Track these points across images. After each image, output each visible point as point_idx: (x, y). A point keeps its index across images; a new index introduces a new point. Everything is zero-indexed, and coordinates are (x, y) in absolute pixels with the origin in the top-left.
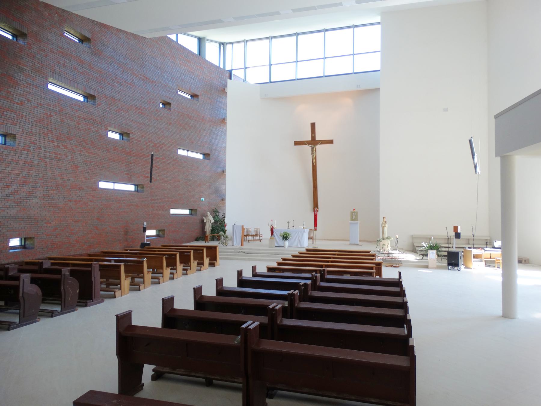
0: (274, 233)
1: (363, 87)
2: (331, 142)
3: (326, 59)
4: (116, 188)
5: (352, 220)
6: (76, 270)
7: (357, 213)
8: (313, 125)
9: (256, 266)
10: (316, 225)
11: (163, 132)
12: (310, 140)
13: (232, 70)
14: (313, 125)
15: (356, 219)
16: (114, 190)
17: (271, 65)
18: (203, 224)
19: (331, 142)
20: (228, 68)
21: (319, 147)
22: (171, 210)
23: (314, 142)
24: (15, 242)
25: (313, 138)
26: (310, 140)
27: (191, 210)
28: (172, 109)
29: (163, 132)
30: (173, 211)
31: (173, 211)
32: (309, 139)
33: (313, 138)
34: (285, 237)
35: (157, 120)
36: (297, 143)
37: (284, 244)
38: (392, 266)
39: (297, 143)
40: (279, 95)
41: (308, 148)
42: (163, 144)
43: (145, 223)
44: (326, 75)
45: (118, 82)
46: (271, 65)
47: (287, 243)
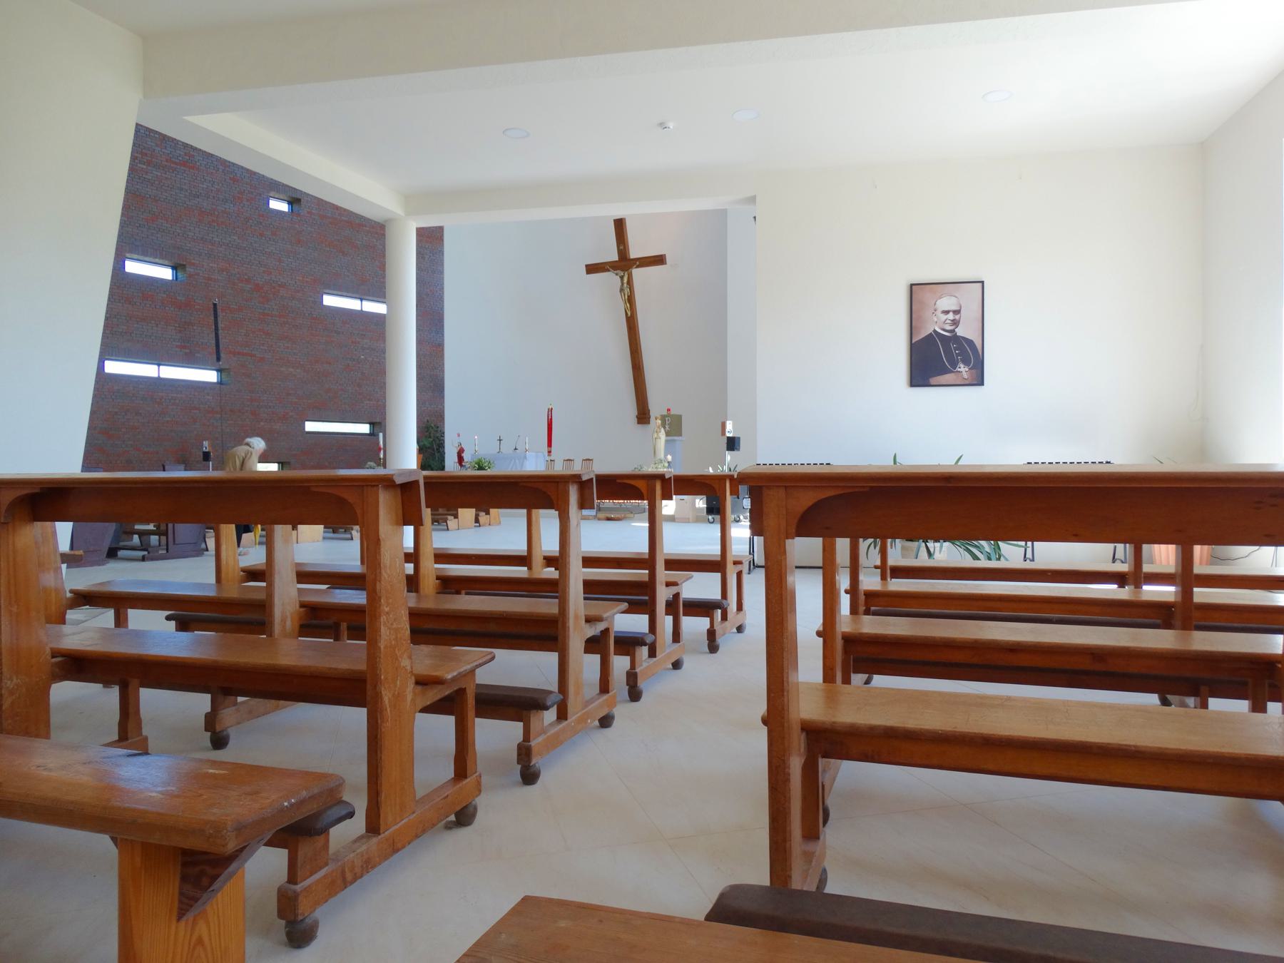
4: (162, 376)
6: (926, 694)
9: (545, 558)
10: (550, 444)
11: (280, 261)
12: (616, 258)
16: (159, 378)
19: (659, 260)
22: (307, 424)
23: (624, 263)
26: (616, 258)
27: (372, 424)
29: (280, 261)
30: (311, 426)
31: (311, 426)
35: (262, 235)
38: (609, 519)
42: (283, 286)
43: (206, 443)
45: (149, 163)
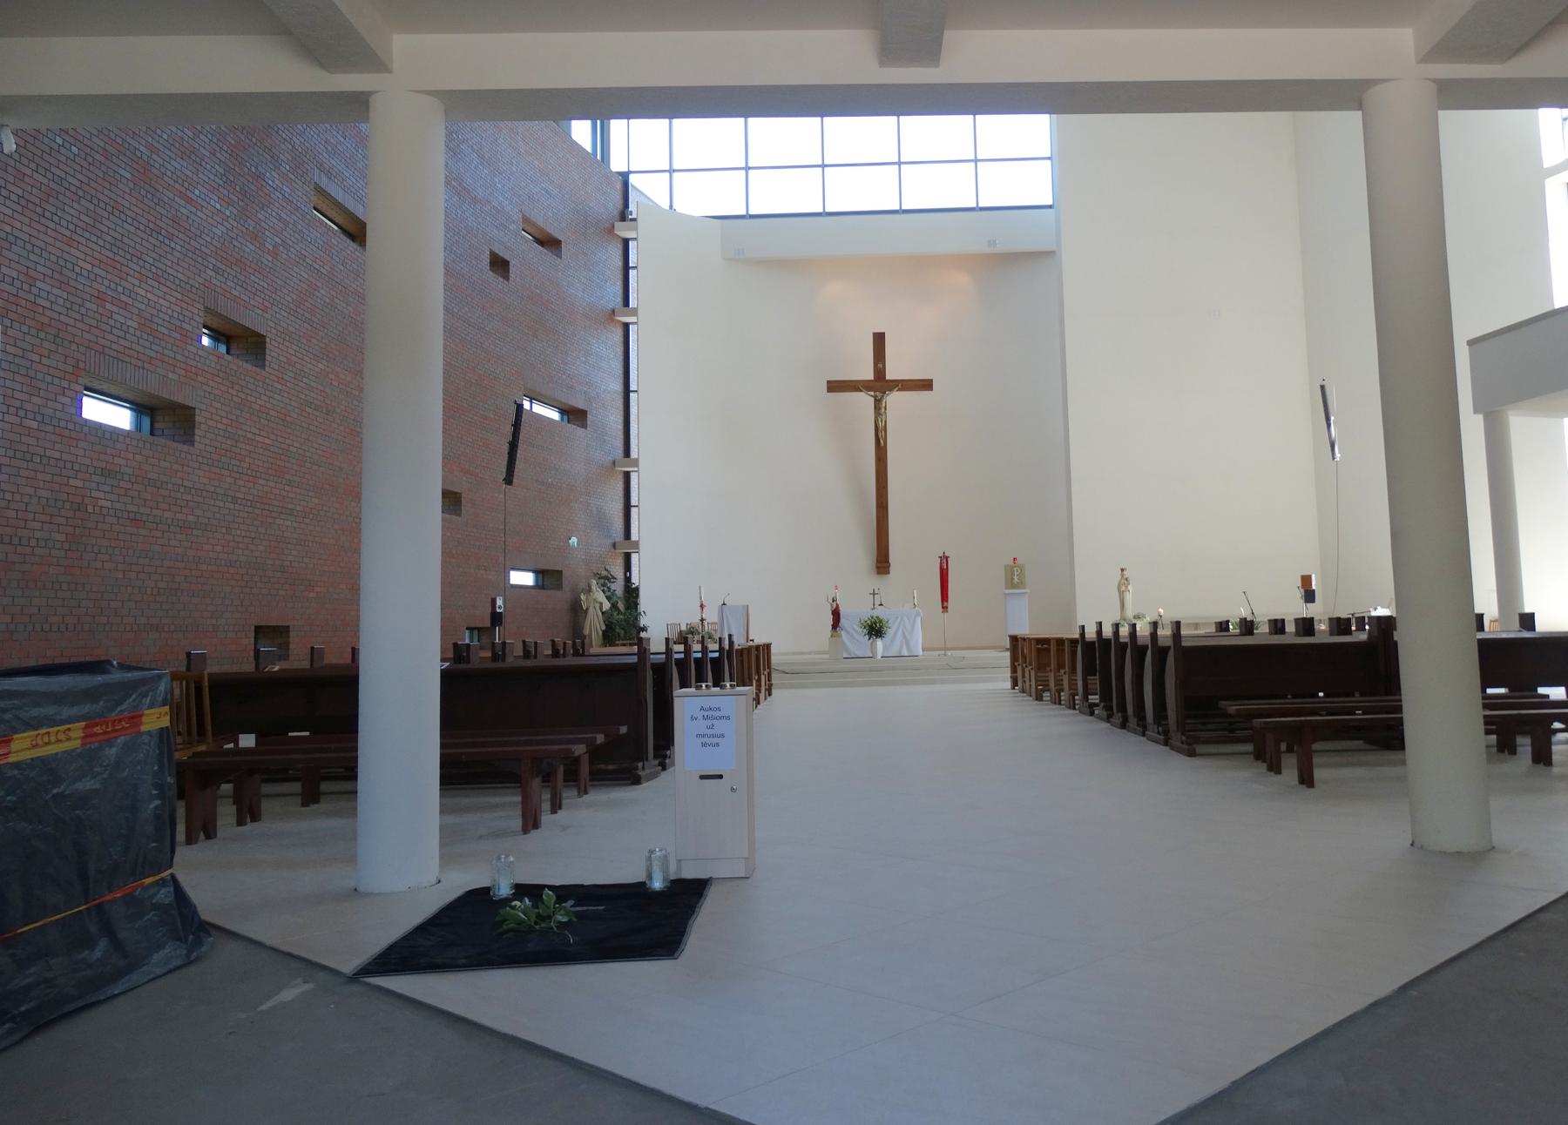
0: (843, 621)
1: (1001, 248)
2: (926, 385)
3: (675, 175)
5: (1011, 584)
7: (1022, 568)
8: (879, 339)
12: (871, 377)
13: (629, 172)
14: (879, 339)
15: (1021, 585)
17: (976, 161)
18: (577, 611)
19: (926, 385)
20: (617, 164)
21: (894, 399)
23: (880, 384)
24: (522, 578)
25: (880, 372)
26: (871, 377)
27: (540, 573)
28: (512, 276)
32: (869, 375)
33: (880, 372)
34: (875, 630)
36: (835, 386)
37: (873, 648)
39: (835, 386)
40: (772, 253)
41: (865, 400)
44: (752, 212)
46: (823, 166)
47: (879, 643)
